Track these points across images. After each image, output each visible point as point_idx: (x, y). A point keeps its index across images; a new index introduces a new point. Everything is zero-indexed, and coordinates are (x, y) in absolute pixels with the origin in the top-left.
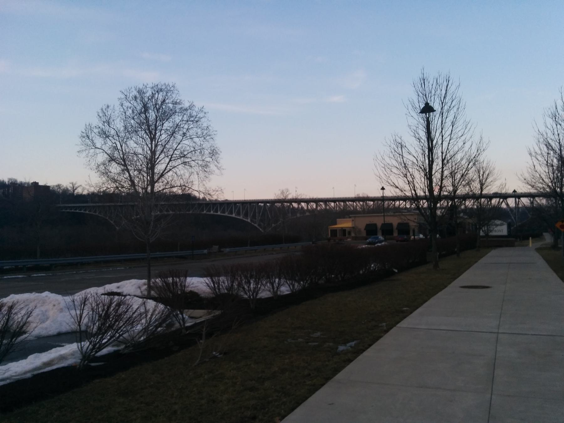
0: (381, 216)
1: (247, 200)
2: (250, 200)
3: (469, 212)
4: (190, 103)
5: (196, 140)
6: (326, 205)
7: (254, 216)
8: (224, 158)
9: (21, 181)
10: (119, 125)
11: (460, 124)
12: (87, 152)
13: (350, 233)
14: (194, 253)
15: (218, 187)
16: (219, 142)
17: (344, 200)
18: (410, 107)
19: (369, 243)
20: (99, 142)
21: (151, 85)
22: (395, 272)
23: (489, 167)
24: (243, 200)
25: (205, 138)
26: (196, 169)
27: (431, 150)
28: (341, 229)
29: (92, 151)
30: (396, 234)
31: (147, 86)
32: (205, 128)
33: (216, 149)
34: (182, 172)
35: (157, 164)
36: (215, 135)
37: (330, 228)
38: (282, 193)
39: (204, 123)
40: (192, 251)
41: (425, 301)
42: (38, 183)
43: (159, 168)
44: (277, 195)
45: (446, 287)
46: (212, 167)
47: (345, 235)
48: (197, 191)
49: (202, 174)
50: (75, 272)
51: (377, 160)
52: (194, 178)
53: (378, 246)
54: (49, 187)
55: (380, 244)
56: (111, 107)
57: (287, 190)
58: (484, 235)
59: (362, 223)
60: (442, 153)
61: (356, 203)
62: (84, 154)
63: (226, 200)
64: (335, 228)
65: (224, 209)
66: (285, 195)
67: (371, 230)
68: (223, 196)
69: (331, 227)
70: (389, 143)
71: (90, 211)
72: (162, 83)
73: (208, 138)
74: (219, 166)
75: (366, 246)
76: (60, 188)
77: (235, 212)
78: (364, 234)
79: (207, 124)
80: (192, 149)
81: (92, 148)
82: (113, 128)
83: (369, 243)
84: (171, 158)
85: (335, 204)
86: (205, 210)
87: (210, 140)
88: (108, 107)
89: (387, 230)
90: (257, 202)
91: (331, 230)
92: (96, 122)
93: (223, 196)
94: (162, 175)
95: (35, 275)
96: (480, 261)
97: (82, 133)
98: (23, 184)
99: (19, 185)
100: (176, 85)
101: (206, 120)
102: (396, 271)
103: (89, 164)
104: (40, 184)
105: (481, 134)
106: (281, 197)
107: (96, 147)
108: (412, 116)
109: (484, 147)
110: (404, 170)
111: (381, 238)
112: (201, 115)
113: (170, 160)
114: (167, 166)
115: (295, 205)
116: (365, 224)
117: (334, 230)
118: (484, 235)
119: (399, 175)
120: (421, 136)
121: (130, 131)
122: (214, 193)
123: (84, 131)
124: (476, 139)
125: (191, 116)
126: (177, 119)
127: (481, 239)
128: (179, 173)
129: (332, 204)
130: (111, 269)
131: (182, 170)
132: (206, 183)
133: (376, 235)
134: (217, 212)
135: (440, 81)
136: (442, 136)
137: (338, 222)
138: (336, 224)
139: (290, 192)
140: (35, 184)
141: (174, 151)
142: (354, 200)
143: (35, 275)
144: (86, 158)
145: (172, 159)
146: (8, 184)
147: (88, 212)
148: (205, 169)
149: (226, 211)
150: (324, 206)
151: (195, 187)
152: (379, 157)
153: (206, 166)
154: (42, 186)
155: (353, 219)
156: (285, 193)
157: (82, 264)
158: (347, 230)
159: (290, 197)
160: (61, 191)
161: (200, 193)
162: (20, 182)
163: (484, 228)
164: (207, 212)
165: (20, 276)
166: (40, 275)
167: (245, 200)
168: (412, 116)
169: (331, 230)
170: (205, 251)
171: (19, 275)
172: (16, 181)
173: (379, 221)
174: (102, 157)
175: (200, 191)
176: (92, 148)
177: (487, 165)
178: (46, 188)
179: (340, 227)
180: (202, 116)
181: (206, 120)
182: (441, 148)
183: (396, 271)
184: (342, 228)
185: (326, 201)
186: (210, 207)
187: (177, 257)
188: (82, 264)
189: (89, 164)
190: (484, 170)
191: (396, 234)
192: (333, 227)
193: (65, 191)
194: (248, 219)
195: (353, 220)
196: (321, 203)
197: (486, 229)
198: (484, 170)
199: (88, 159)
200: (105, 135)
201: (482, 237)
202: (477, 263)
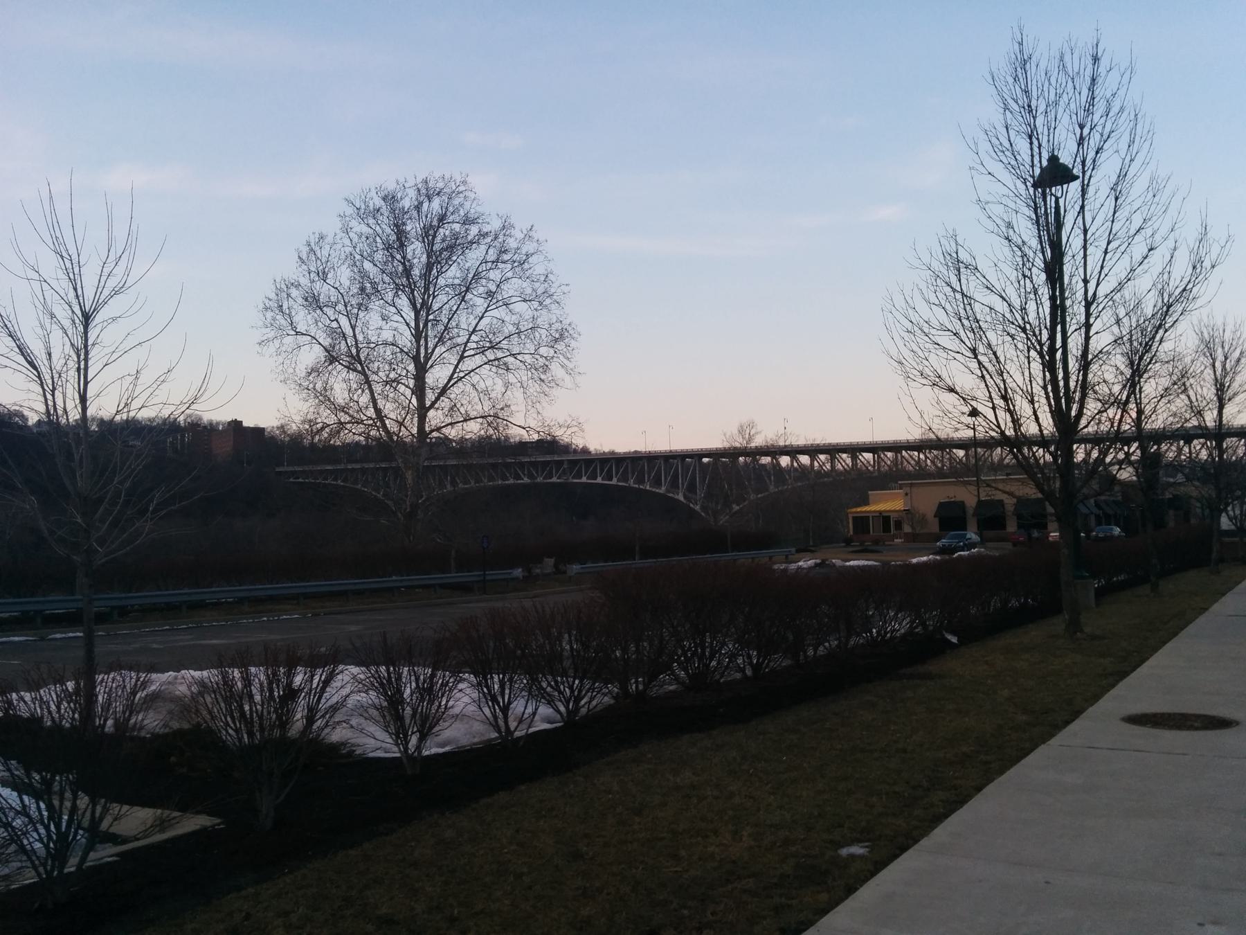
0: (969, 483)
1: (676, 451)
2: (682, 451)
3: (1194, 469)
4: (501, 218)
5: (520, 307)
6: (854, 458)
7: (692, 488)
8: (584, 351)
9: (209, 419)
10: (344, 276)
11: (1136, 191)
12: (277, 342)
13: (899, 525)
14: (488, 578)
15: (570, 416)
16: (574, 311)
17: (896, 447)
18: (984, 146)
19: (942, 551)
20: (303, 319)
21: (411, 183)
22: (949, 642)
23: (1240, 343)
24: (666, 452)
25: (541, 303)
26: (524, 375)
27: (1054, 270)
28: (878, 514)
29: (288, 340)
30: (1012, 527)
31: (406, 185)
32: (542, 278)
33: (569, 328)
34: (489, 383)
35: (432, 366)
36: (564, 293)
37: (851, 513)
38: (741, 431)
39: (537, 267)
40: (482, 573)
41: (960, 801)
42: (241, 422)
43: (437, 376)
44: (730, 436)
45: (1076, 714)
46: (556, 370)
47: (886, 528)
48: (524, 428)
49: (534, 388)
50: (168, 627)
51: (894, 311)
52: (516, 397)
53: (799, 568)
54: (263, 429)
55: (966, 553)
56: (329, 239)
57: (751, 425)
58: (1233, 527)
59: (929, 500)
60: (1086, 281)
61: (925, 454)
62: (272, 348)
63: (613, 453)
64: (865, 512)
65: (626, 471)
66: (747, 436)
67: (951, 517)
68: (583, 438)
69: (854, 510)
70: (926, 259)
71: (335, 479)
72: (437, 175)
73: (548, 301)
74: (570, 365)
75: (931, 556)
76: (284, 432)
77: (617, 474)
78: (934, 527)
79: (546, 270)
80: (512, 329)
81: (288, 335)
82: (333, 287)
83: (942, 551)
84: (464, 351)
85: (876, 456)
86: (600, 476)
87: (553, 307)
88: (322, 238)
89: (991, 518)
90: (682, 456)
91: (855, 519)
92: (293, 271)
93: (583, 438)
94: (443, 391)
95: (58, 636)
96: (1216, 607)
97: (267, 301)
98: (214, 424)
99: (205, 427)
100: (469, 180)
101: (542, 258)
102: (954, 640)
103: (282, 370)
104: (245, 424)
105: (1204, 216)
106: (739, 442)
107: (297, 330)
108: (990, 173)
109: (1214, 256)
110: (968, 338)
111: (972, 536)
112: (529, 247)
113: (462, 358)
114: (454, 372)
115: (785, 461)
116: (938, 503)
117: (862, 518)
118: (1233, 527)
119: (958, 352)
120: (1026, 239)
121: (367, 292)
122: (563, 430)
123: (273, 296)
124: (1190, 235)
125: (503, 251)
126: (474, 256)
127: (1227, 540)
128: (482, 386)
129: (868, 456)
130: (265, 619)
131: (488, 378)
132: (543, 407)
133: (965, 529)
134: (611, 479)
135: (1073, 64)
136: (1085, 231)
137: (871, 501)
138: (867, 504)
139: (759, 429)
140: (236, 425)
141: (470, 336)
142: (920, 446)
143: (58, 636)
144: (276, 358)
145: (466, 355)
146: (185, 426)
147: (343, 481)
148: (543, 377)
149: (630, 476)
150: (849, 461)
151: (518, 419)
152: (900, 302)
153: (546, 368)
154: (249, 427)
155: (908, 490)
156: (748, 431)
157: (272, 599)
158: (891, 517)
159: (758, 442)
160: (287, 439)
161: (531, 433)
162: (208, 420)
163: (1233, 510)
164: (544, 479)
165: (16, 639)
166: (71, 635)
167: (671, 451)
168: (990, 173)
169: (855, 519)
170: (518, 572)
171: (14, 636)
172: (201, 419)
173: (968, 496)
174: (312, 355)
175: (529, 427)
176: (288, 335)
177: (1235, 337)
178: (258, 431)
179: (875, 512)
180: (532, 251)
181: (542, 258)
182: (1081, 270)
183: (954, 640)
184: (880, 512)
185: (854, 450)
186: (595, 469)
187: (443, 586)
188: (197, 606)
189: (282, 370)
190: (1226, 349)
191: (1012, 527)
192: (859, 509)
193: (296, 439)
194: (470, 483)
195: (906, 494)
196: (844, 456)
197: (1238, 512)
198: (1226, 349)
199: (281, 359)
200: (313, 302)
201: (1228, 533)
202: (1207, 614)
